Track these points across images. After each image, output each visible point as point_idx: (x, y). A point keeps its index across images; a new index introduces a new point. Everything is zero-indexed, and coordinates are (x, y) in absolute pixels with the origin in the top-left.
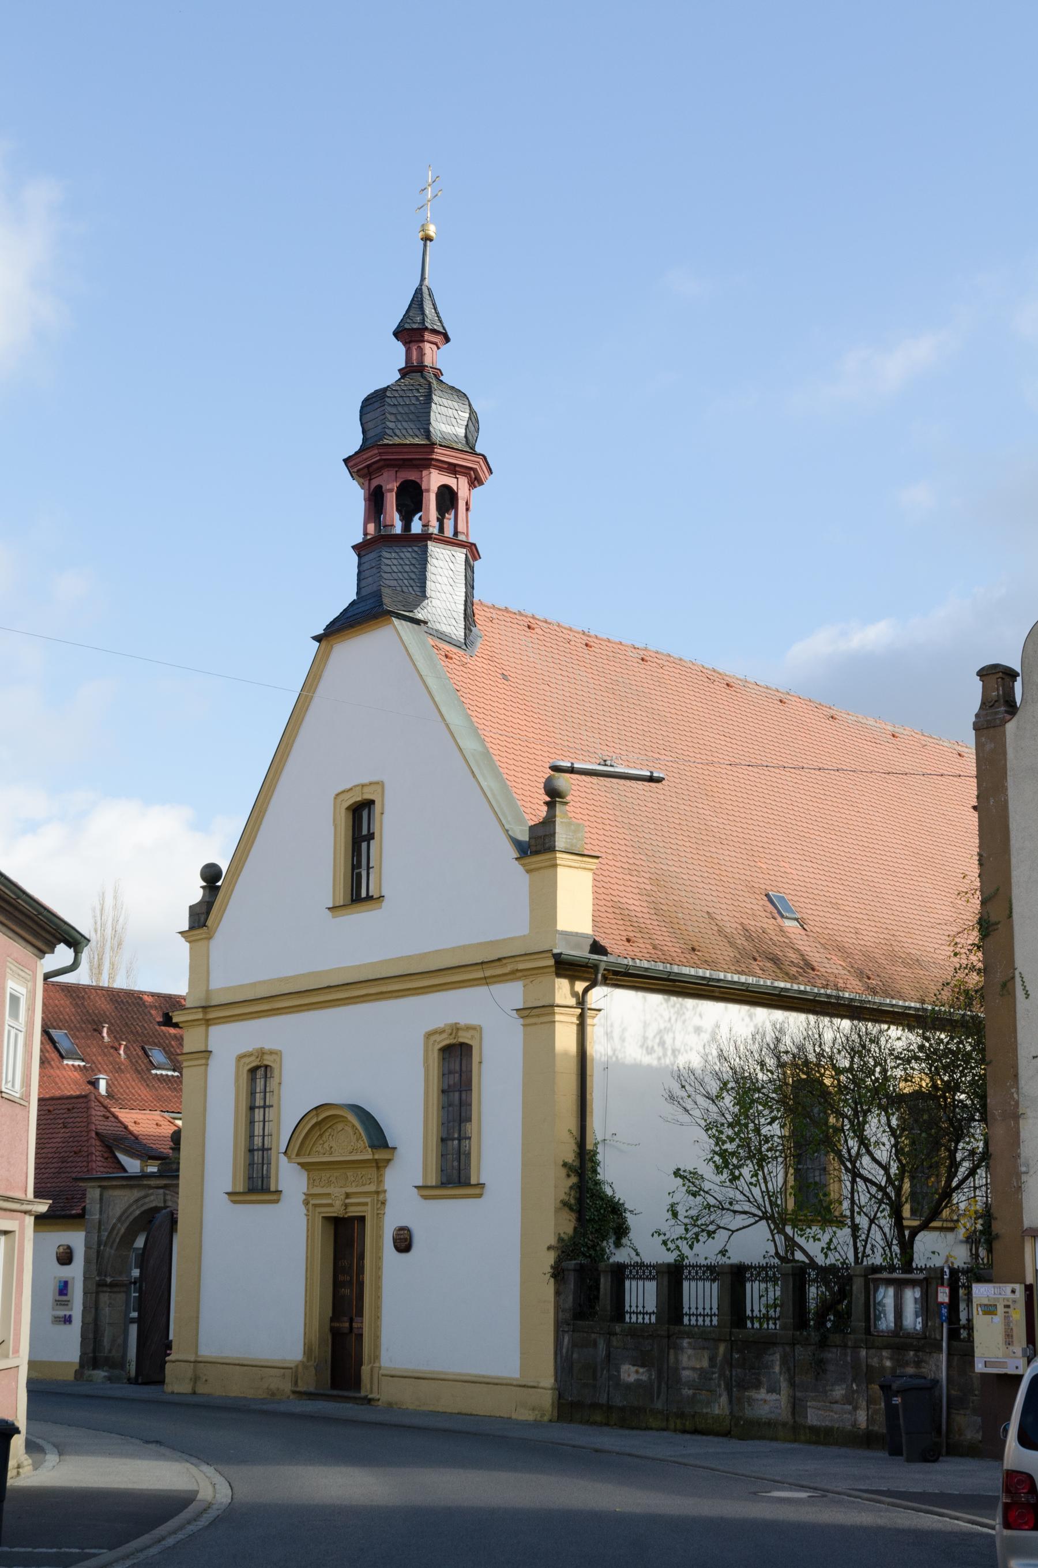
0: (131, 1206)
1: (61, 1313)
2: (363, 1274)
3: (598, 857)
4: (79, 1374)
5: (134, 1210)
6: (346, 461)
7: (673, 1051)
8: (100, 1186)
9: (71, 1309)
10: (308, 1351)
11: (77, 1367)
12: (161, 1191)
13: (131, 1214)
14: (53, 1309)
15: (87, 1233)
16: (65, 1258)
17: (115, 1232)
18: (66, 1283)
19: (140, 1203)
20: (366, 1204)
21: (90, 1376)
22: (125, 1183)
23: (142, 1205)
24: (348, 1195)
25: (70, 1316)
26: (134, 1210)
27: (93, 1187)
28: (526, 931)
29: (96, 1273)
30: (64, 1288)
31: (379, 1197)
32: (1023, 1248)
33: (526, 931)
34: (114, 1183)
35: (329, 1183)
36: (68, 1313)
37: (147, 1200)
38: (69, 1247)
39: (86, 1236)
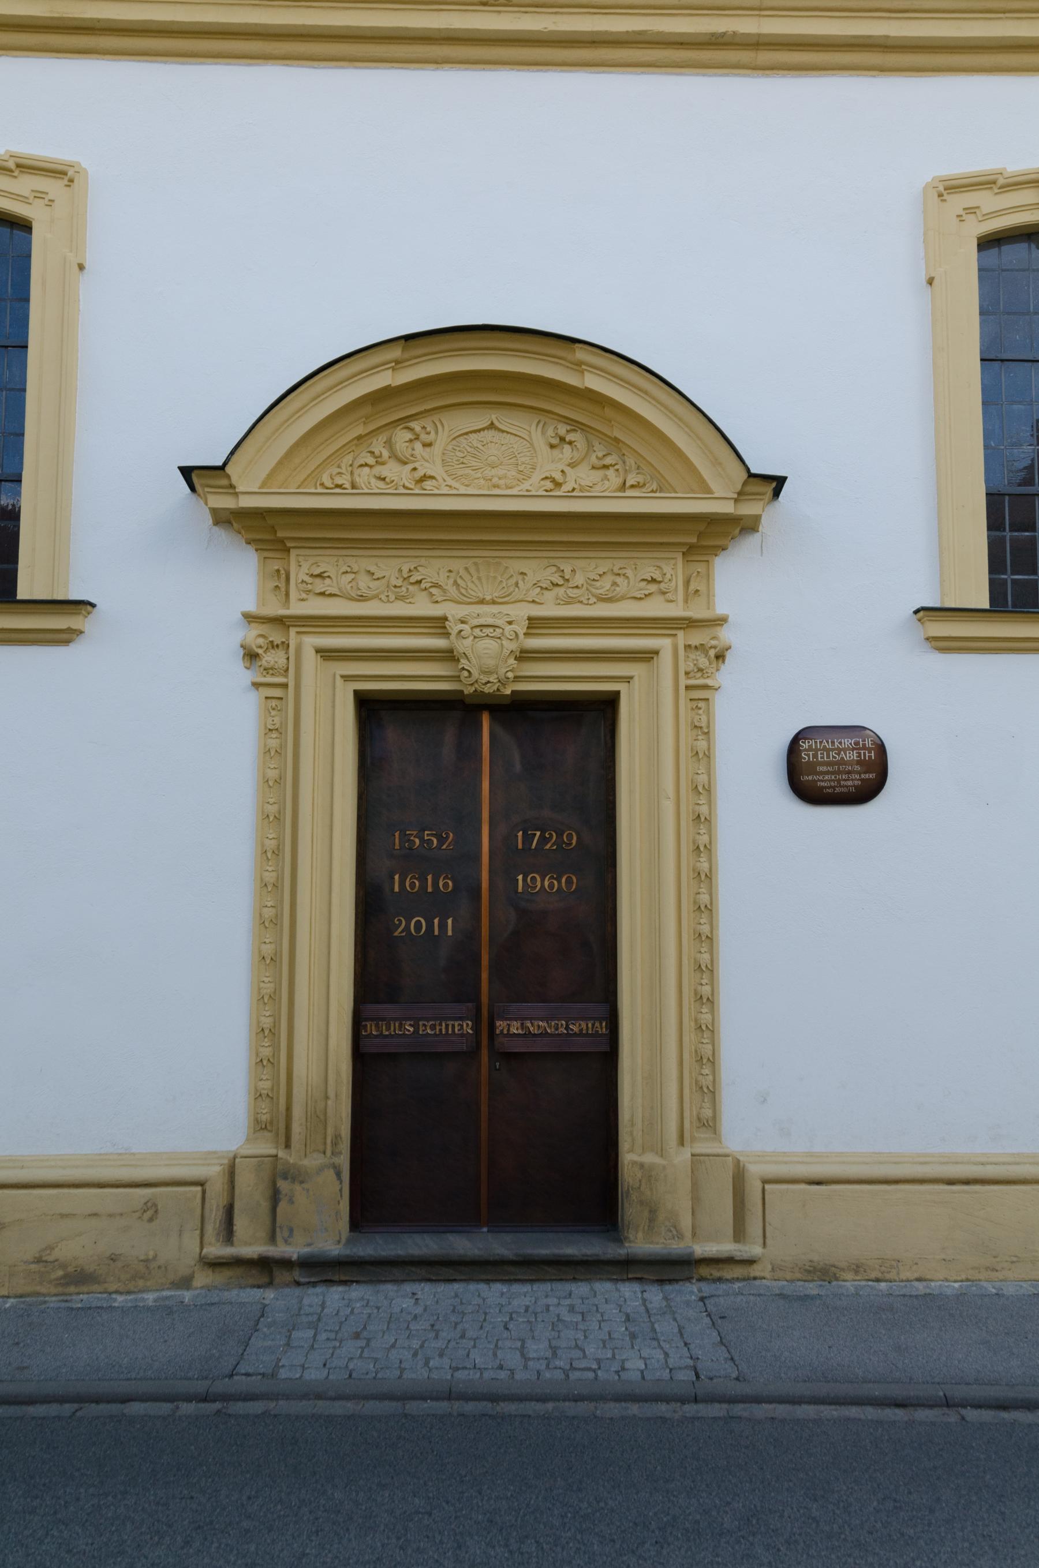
10: (273, 1117)
20: (648, 656)
24: (535, 624)
31: (704, 642)
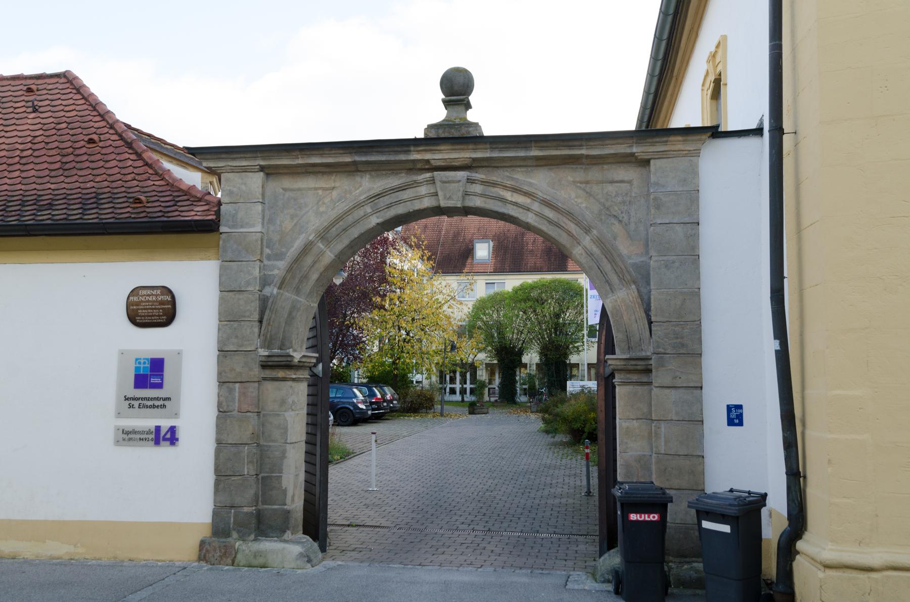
0: (358, 206)
3: (261, 322)
4: (204, 552)
5: (366, 216)
7: (677, 338)
8: (262, 169)
9: (176, 415)
11: (206, 533)
12: (462, 175)
13: (357, 222)
14: (119, 415)
15: (226, 262)
16: (154, 310)
17: (309, 260)
18: (157, 365)
19: (387, 200)
21: (257, 554)
23: (389, 206)
25: (172, 430)
26: (366, 216)
27: (244, 170)
29: (258, 342)
32: (777, 574)
36: (165, 424)
37: (405, 195)
38: (167, 291)
39: (222, 268)
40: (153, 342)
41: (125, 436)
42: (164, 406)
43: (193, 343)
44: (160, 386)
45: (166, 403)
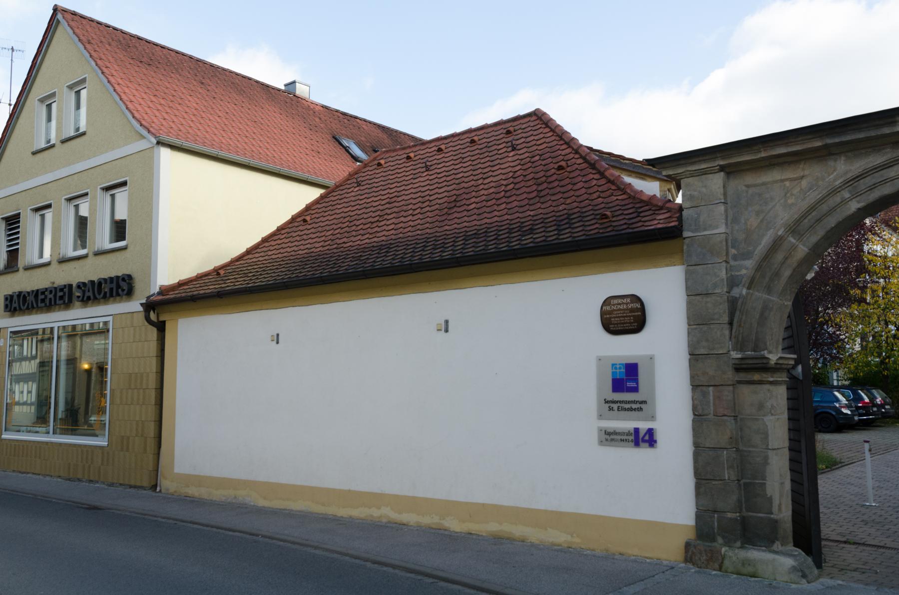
1: (626, 424)
2: (636, 177)
4: (690, 553)
5: (844, 202)
6: (651, 358)
8: (722, 168)
9: (653, 418)
14: (600, 417)
17: (780, 256)
18: (632, 370)
22: (818, 144)
25: (650, 432)
26: (844, 202)
28: (177, 469)
30: (626, 379)
33: (177, 469)
34: (782, 150)
35: (803, 169)
36: (643, 426)
40: (626, 347)
41: (607, 437)
42: (641, 409)
43: (665, 347)
44: (635, 390)
45: (643, 406)
